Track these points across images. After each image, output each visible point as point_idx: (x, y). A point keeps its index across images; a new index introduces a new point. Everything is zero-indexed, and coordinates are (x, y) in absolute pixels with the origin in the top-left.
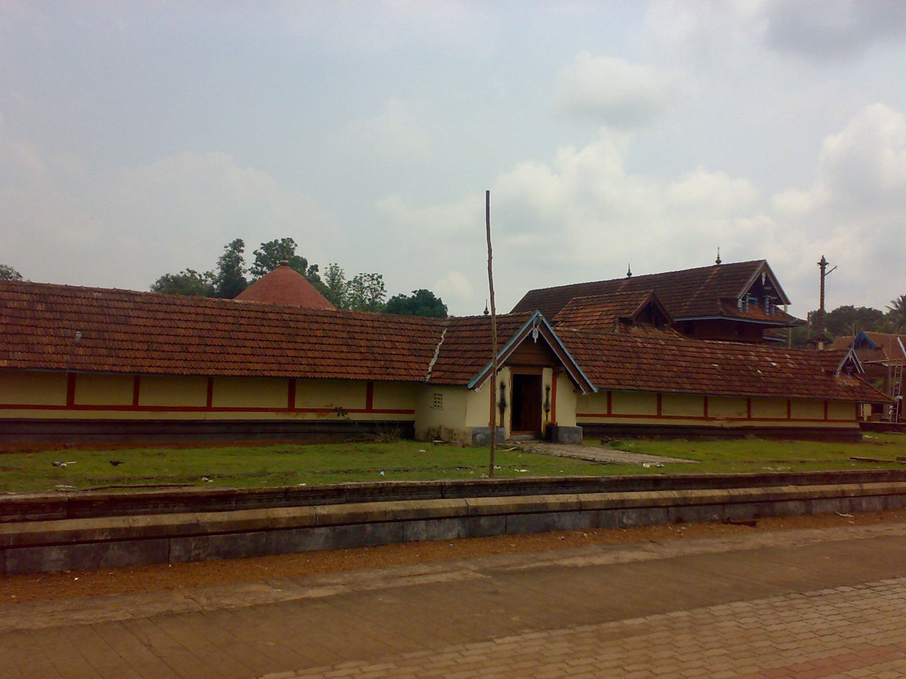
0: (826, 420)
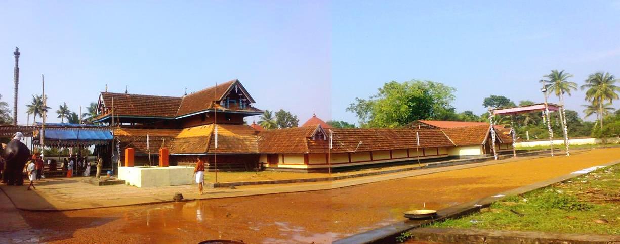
0: (409, 157)
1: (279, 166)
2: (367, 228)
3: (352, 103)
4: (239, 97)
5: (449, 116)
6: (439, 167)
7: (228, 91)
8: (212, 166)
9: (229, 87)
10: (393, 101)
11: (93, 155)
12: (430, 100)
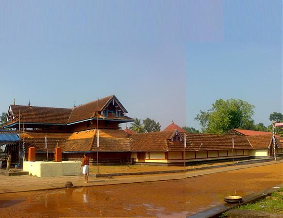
1: (146, 161)
2: (203, 208)
4: (115, 108)
5: (250, 127)
6: (244, 164)
8: (95, 161)
10: (220, 114)
11: (4, 153)
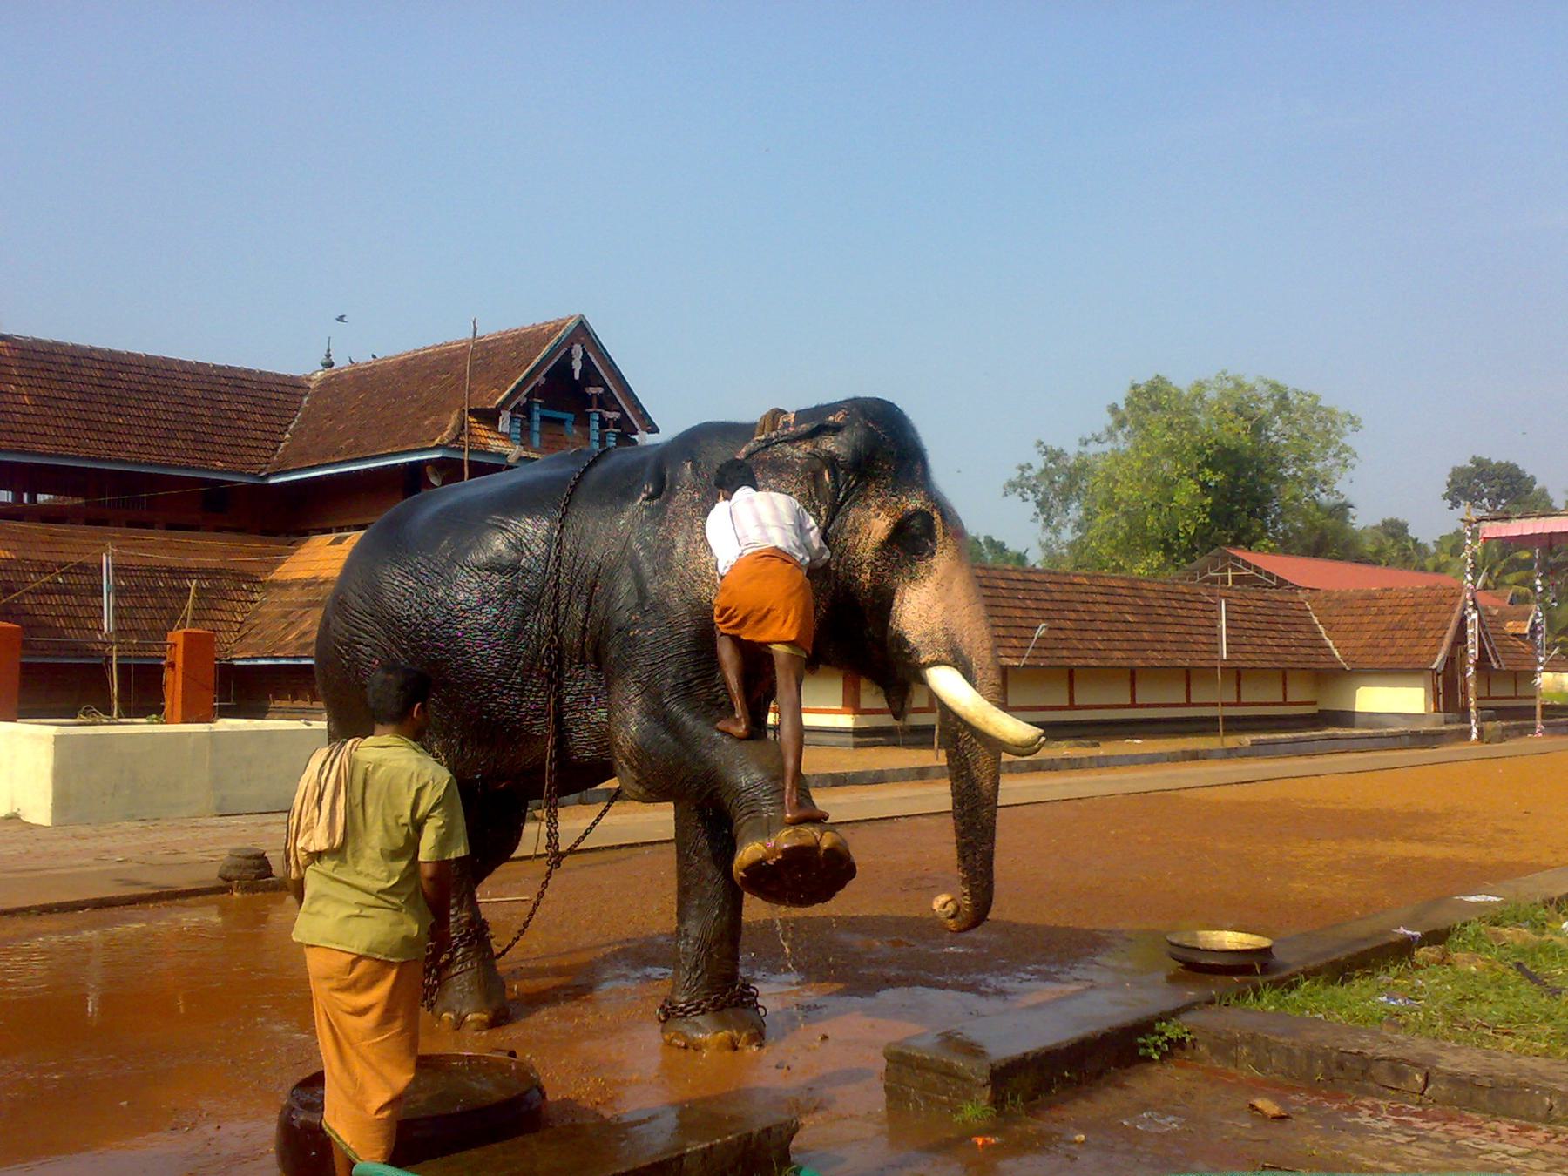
3: (1024, 463)
4: (587, 401)
5: (1328, 538)
7: (539, 366)
9: (546, 350)
12: (1272, 462)
